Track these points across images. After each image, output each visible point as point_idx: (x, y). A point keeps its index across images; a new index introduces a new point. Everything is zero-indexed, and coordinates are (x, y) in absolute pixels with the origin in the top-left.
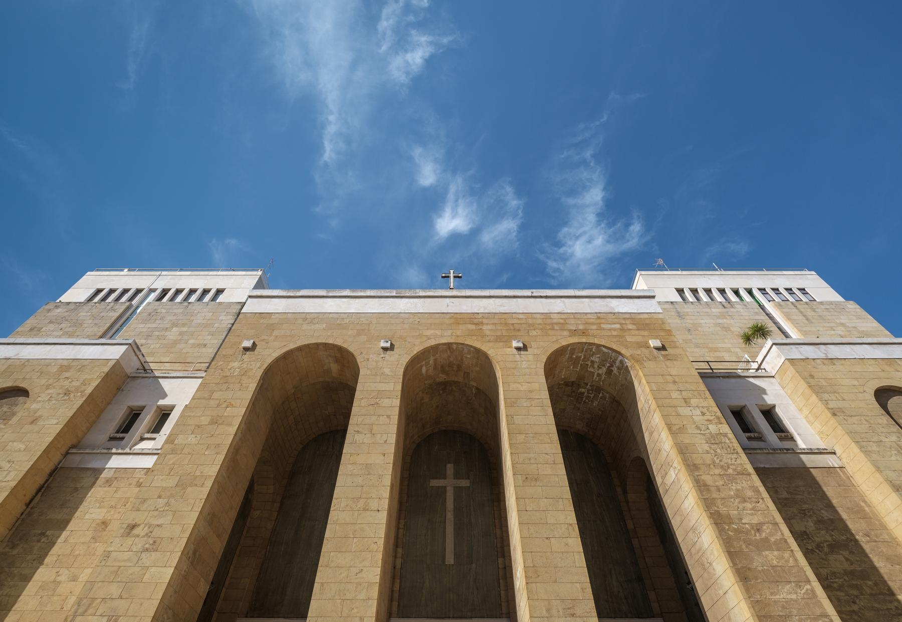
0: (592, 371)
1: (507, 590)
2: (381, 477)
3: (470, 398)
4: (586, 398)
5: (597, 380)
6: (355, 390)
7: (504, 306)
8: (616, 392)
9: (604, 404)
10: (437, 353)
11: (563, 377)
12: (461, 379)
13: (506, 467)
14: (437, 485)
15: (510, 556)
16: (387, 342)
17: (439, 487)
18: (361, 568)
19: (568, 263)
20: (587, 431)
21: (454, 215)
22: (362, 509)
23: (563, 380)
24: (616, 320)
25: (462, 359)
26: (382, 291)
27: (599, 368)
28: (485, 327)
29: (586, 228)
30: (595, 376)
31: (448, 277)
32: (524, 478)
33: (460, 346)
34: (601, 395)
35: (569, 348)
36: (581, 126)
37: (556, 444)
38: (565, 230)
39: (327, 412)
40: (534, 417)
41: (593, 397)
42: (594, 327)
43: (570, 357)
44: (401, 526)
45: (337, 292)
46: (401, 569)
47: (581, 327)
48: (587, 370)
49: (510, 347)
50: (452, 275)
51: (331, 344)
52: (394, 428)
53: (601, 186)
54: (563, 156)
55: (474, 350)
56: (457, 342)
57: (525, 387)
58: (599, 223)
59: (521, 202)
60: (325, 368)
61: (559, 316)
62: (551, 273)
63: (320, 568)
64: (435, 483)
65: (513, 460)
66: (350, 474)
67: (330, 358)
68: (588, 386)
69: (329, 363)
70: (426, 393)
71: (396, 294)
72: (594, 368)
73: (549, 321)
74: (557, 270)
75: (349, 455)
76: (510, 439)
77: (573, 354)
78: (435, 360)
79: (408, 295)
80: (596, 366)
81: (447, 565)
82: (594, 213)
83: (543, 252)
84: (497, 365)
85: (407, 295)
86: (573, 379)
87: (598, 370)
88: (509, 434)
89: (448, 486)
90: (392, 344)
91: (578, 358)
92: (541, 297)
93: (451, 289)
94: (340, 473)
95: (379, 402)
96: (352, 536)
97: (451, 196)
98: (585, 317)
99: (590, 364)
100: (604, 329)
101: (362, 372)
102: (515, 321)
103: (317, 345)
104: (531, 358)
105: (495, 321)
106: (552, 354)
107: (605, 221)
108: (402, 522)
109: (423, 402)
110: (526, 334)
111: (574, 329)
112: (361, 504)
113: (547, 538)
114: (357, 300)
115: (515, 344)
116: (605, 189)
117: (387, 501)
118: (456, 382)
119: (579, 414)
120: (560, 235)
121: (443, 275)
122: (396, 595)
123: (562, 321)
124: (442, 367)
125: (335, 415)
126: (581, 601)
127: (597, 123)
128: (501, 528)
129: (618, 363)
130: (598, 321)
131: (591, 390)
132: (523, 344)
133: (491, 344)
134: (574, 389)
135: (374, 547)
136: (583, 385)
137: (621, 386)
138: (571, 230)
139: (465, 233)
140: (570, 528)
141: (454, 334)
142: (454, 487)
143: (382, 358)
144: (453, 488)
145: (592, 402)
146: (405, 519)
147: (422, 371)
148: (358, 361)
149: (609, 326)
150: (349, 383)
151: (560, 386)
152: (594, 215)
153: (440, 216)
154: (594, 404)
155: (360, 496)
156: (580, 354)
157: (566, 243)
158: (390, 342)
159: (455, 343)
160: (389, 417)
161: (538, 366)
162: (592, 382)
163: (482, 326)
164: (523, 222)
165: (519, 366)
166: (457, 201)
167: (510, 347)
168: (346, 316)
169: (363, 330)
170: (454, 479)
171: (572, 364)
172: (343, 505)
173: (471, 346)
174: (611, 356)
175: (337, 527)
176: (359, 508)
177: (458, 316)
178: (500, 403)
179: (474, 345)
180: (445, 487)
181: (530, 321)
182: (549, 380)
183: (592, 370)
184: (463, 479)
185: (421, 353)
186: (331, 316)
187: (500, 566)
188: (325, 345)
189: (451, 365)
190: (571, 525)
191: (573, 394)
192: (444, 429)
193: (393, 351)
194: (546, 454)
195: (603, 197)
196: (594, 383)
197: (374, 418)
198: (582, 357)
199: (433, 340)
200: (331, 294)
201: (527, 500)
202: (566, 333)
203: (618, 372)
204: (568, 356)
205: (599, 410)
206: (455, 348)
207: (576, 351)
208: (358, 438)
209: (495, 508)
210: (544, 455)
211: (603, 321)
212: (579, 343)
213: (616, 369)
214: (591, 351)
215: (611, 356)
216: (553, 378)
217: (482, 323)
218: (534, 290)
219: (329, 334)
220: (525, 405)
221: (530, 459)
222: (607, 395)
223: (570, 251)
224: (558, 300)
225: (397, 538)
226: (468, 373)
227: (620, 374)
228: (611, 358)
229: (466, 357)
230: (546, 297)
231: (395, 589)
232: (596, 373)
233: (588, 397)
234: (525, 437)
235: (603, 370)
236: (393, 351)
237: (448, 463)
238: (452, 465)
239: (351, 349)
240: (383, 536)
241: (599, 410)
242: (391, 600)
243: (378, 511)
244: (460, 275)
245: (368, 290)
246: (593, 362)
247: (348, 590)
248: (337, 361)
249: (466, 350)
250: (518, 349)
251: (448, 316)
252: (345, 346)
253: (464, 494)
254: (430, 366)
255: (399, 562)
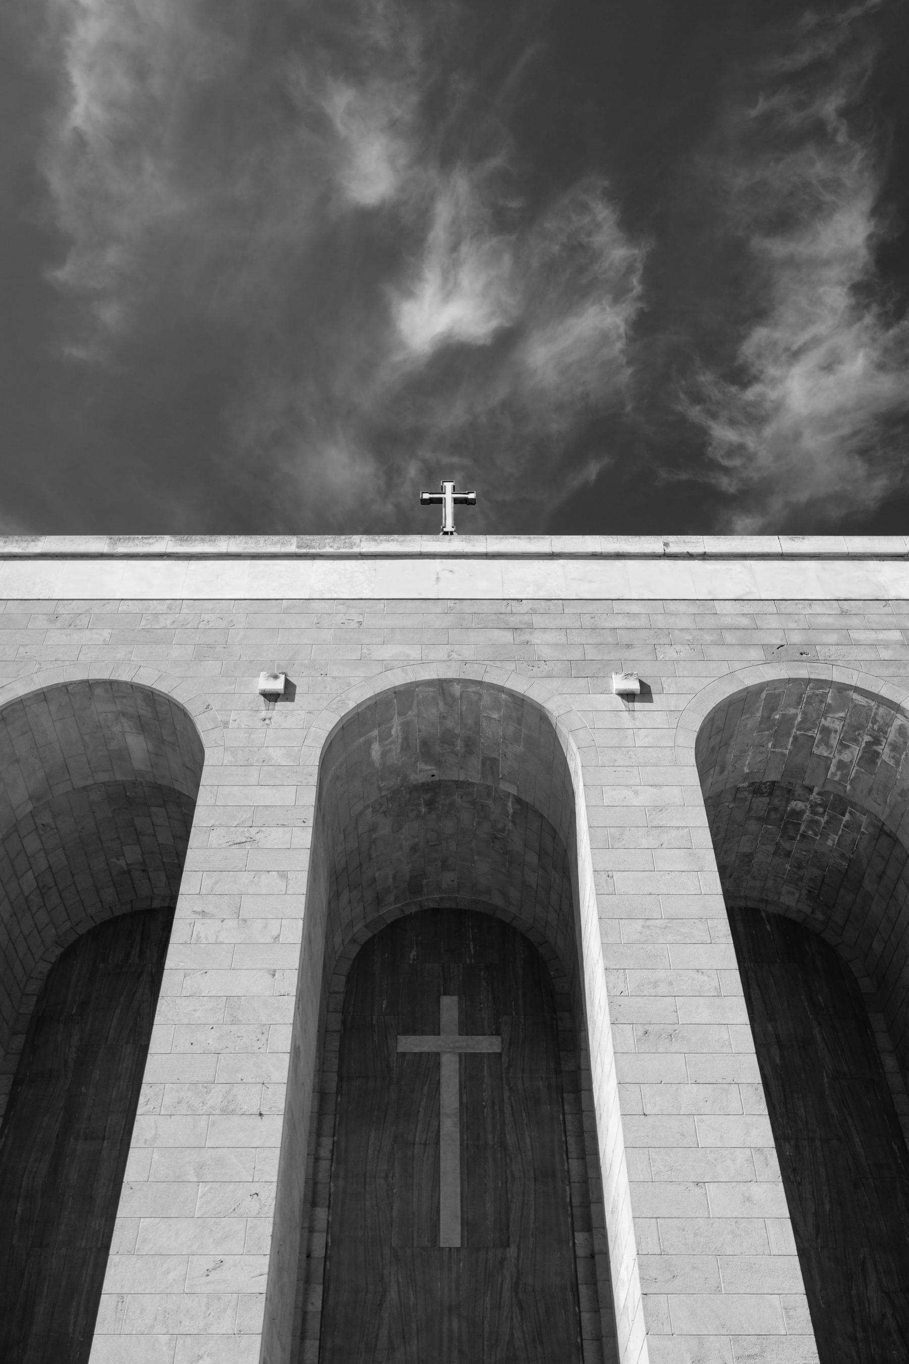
0: (826, 754)
1: (596, 1311)
2: (264, 1029)
3: (500, 826)
4: (808, 827)
5: (837, 778)
6: (195, 806)
7: (590, 582)
8: (887, 811)
9: (854, 841)
10: (410, 708)
11: (746, 770)
12: (475, 777)
13: (592, 1002)
14: (416, 1050)
15: (603, 1227)
16: (276, 677)
17: (421, 1054)
18: (221, 1257)
19: (768, 431)
20: (808, 910)
21: (449, 292)
22: (217, 1112)
23: (746, 777)
24: (892, 620)
25: (477, 723)
26: (261, 539)
27: (843, 746)
28: (537, 638)
29: (819, 329)
30: (833, 769)
31: (440, 501)
32: (640, 1033)
33: (473, 689)
34: (847, 817)
35: (764, 695)
36: (809, 19)
37: (723, 946)
38: (760, 334)
39: (122, 862)
40: (668, 877)
41: (827, 822)
42: (832, 638)
43: (767, 720)
44: (325, 1152)
45: (136, 542)
46: (325, 1257)
47: (796, 638)
48: (811, 753)
49: (606, 691)
50: (449, 497)
51: (126, 683)
52: (297, 906)
53: (865, 204)
54: (754, 113)
55: (509, 699)
56: (462, 677)
57: (646, 797)
58: (857, 311)
59: (636, 251)
60: (113, 746)
61: (737, 607)
62: (720, 460)
63: (113, 1259)
64: (409, 1044)
65: (610, 985)
66: (186, 1021)
67: (124, 720)
68: (814, 794)
69: (123, 733)
70: (384, 813)
71: (298, 547)
72: (829, 746)
73: (710, 622)
74: (739, 449)
75: (182, 973)
76: (604, 934)
77: (773, 709)
78: (406, 726)
79: (331, 550)
80: (834, 741)
81: (443, 1248)
82: (842, 284)
83: (697, 398)
84: (571, 741)
85: (328, 550)
86: (773, 776)
87: (840, 752)
88: (600, 918)
89: (446, 1052)
90: (288, 684)
91: (788, 720)
92: (690, 556)
93: (446, 533)
94: (158, 1019)
95: (257, 837)
96: (195, 1179)
97: (439, 235)
98: (808, 611)
99: (818, 737)
100: (857, 644)
101: (211, 758)
102: (621, 622)
103: (89, 686)
104: (660, 719)
105: (566, 622)
106: (717, 709)
107: (875, 308)
108: (327, 1142)
109: (374, 836)
110: (650, 658)
111: (779, 642)
112: (215, 1098)
113: (697, 1184)
114: (194, 564)
115: (619, 683)
116: (876, 212)
117: (283, 1090)
118: (463, 782)
119: (788, 867)
120: (748, 349)
121: (426, 496)
122: (314, 1325)
123: (745, 622)
124: (424, 743)
125: (143, 871)
126: (783, 1339)
127: (855, 11)
128: (582, 1157)
129: (892, 734)
130: (843, 622)
131: (820, 805)
132: (642, 683)
133: (555, 683)
134: (776, 802)
135: (253, 1205)
136: (799, 791)
137: (900, 795)
138: (777, 335)
139: (481, 342)
140: (756, 1157)
141: (454, 656)
142: (460, 1054)
143: (265, 720)
144: (457, 1059)
145: (825, 836)
146: (334, 1136)
147: (370, 754)
148: (200, 728)
149: (872, 636)
150: (177, 787)
151: (739, 795)
152: (845, 289)
153: (409, 294)
154: (830, 843)
155: (210, 1079)
156: (792, 711)
157: (761, 372)
158: (282, 677)
159: (459, 681)
160: (283, 874)
161: (680, 741)
162: (824, 786)
163: (531, 633)
164: (642, 310)
165: (630, 743)
166: (455, 248)
167: (606, 691)
168: (163, 607)
169: (210, 646)
170: (460, 1034)
171: (770, 736)
172: (167, 1100)
173: (501, 689)
174: (876, 714)
175: (156, 1156)
176: (212, 1107)
177: (466, 607)
178: (578, 838)
179: (508, 685)
180: (438, 1054)
181: (660, 621)
182: (710, 780)
183: (822, 751)
184: (483, 1034)
185: (368, 708)
186: (123, 607)
187: (580, 1252)
188: (111, 685)
189: (447, 738)
190: (759, 1150)
191: (773, 816)
192: (433, 905)
193: (293, 700)
194: (698, 970)
195: (870, 237)
196: (828, 788)
197: (245, 878)
198: (799, 719)
199: (398, 672)
200: (121, 549)
201: (646, 1089)
202: (755, 654)
203: (893, 757)
204: (759, 714)
205: (842, 856)
206: (458, 694)
207: (783, 702)
208: (206, 930)
209: (566, 1107)
210: (693, 974)
211: (855, 621)
212: (789, 680)
213: (887, 750)
214: (822, 702)
215: (876, 714)
216: (722, 772)
217: (531, 627)
218: (671, 539)
219: (119, 656)
220: (644, 843)
221: (655, 984)
222: (864, 819)
223: (773, 395)
224: (737, 566)
225: (315, 1183)
226: (495, 761)
227: (897, 763)
228: (875, 721)
229: (489, 719)
230: (704, 556)
231: (310, 1308)
232: (834, 761)
233: (813, 823)
234: (643, 927)
235: (854, 753)
236: (293, 700)
237: (445, 994)
238: (455, 998)
239: (181, 696)
240: (275, 1179)
241: (842, 856)
242: (301, 1335)
243: (261, 1115)
244: (472, 496)
245: (223, 537)
246: (826, 731)
247: (188, 1311)
248: (142, 727)
249: (487, 700)
250: (628, 696)
251: (439, 607)
252: (163, 687)
253: (486, 1073)
254: (392, 743)
255: (319, 1242)
